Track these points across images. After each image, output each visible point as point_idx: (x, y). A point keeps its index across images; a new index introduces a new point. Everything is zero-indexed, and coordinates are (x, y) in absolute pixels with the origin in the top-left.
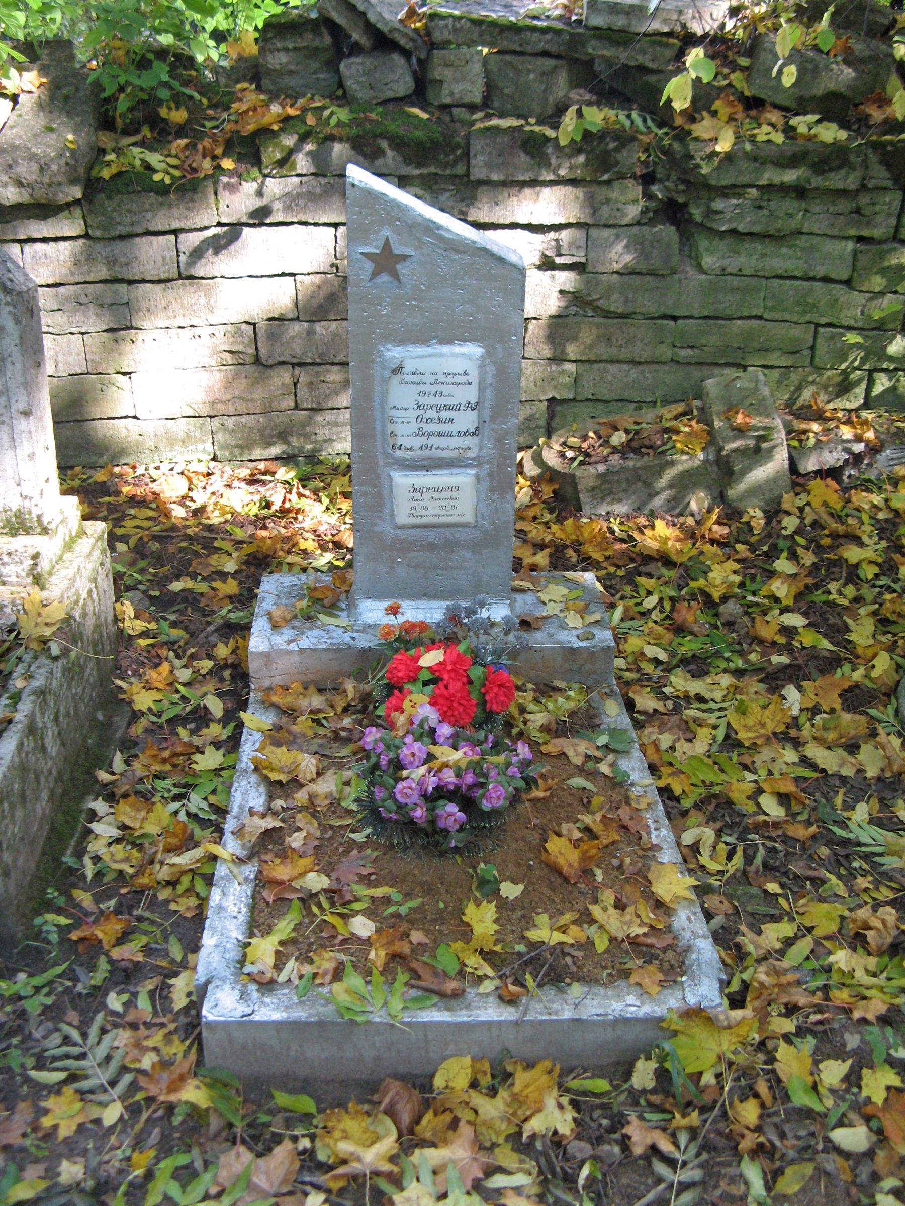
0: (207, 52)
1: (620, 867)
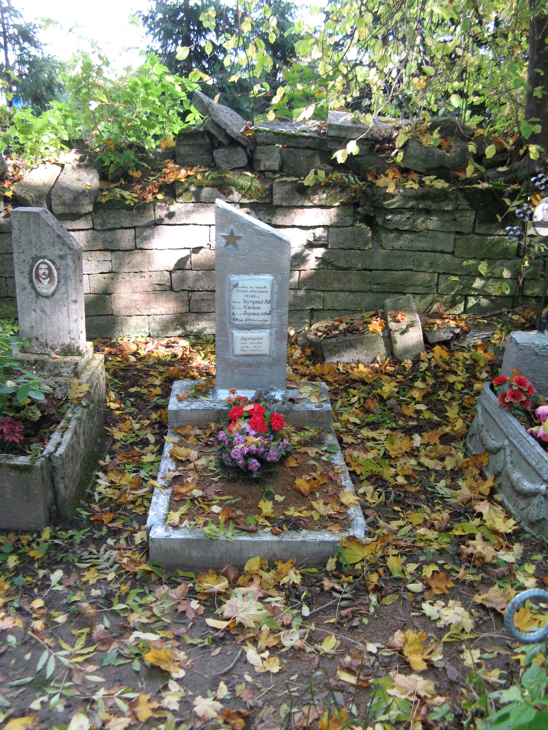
0: (151, 145)
1: (327, 492)
